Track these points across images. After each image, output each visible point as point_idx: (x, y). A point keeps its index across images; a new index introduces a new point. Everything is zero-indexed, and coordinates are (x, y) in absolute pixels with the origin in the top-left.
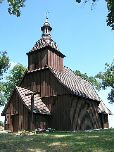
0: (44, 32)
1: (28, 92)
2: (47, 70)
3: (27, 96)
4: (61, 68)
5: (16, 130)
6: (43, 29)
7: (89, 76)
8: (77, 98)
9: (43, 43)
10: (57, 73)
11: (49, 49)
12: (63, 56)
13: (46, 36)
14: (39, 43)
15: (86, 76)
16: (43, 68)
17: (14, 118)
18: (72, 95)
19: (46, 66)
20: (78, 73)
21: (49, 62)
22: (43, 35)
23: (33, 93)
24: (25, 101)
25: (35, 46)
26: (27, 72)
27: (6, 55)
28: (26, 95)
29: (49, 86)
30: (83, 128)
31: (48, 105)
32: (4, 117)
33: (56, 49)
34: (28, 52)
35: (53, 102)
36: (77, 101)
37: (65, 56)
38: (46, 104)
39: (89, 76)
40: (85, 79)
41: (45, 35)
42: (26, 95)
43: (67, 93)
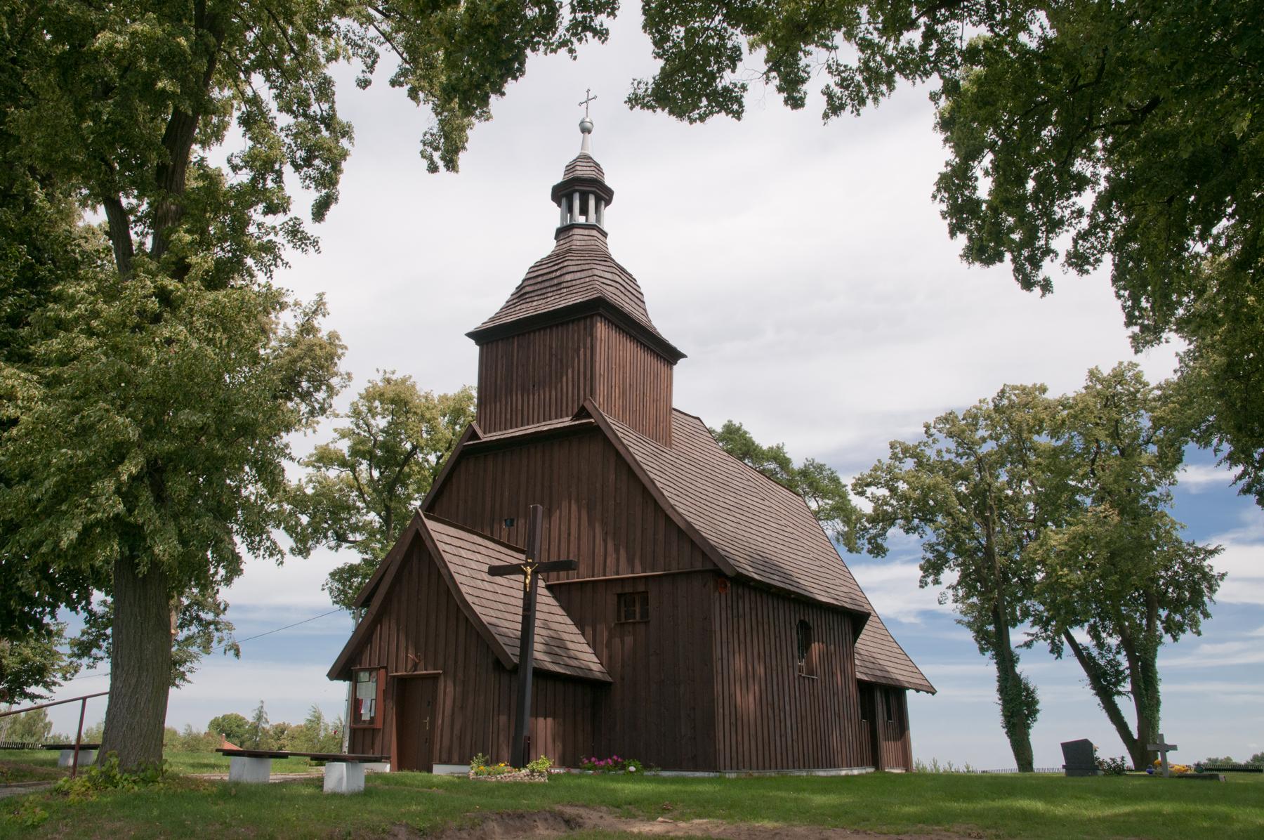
0: (570, 210)
1: (502, 557)
2: (590, 433)
3: (498, 579)
4: (661, 419)
5: (414, 755)
6: (562, 193)
7: (797, 464)
8: (747, 591)
9: (568, 277)
10: (640, 450)
11: (601, 316)
12: (670, 355)
13: (579, 239)
14: (541, 278)
15: (784, 462)
16: (566, 422)
17: (405, 694)
18: (726, 577)
19: (582, 412)
20: (736, 443)
21: (601, 389)
22: (562, 232)
23: (531, 565)
24: (476, 600)
25: (521, 295)
26: (474, 435)
27: (324, 326)
28: (494, 571)
29: (597, 525)
30: (456, 758)
31: (589, 630)
32: (343, 687)
33: (636, 314)
34: (476, 323)
35: (619, 611)
36: (747, 610)
37: (684, 356)
38: (580, 624)
39: (797, 464)
40: (770, 475)
41: (576, 231)
42: (494, 571)
43: (698, 566)
